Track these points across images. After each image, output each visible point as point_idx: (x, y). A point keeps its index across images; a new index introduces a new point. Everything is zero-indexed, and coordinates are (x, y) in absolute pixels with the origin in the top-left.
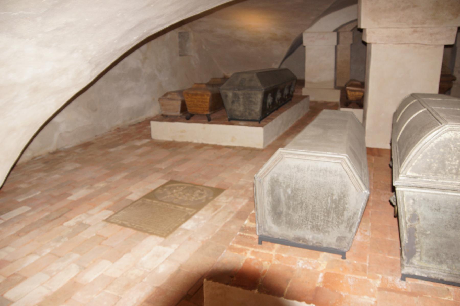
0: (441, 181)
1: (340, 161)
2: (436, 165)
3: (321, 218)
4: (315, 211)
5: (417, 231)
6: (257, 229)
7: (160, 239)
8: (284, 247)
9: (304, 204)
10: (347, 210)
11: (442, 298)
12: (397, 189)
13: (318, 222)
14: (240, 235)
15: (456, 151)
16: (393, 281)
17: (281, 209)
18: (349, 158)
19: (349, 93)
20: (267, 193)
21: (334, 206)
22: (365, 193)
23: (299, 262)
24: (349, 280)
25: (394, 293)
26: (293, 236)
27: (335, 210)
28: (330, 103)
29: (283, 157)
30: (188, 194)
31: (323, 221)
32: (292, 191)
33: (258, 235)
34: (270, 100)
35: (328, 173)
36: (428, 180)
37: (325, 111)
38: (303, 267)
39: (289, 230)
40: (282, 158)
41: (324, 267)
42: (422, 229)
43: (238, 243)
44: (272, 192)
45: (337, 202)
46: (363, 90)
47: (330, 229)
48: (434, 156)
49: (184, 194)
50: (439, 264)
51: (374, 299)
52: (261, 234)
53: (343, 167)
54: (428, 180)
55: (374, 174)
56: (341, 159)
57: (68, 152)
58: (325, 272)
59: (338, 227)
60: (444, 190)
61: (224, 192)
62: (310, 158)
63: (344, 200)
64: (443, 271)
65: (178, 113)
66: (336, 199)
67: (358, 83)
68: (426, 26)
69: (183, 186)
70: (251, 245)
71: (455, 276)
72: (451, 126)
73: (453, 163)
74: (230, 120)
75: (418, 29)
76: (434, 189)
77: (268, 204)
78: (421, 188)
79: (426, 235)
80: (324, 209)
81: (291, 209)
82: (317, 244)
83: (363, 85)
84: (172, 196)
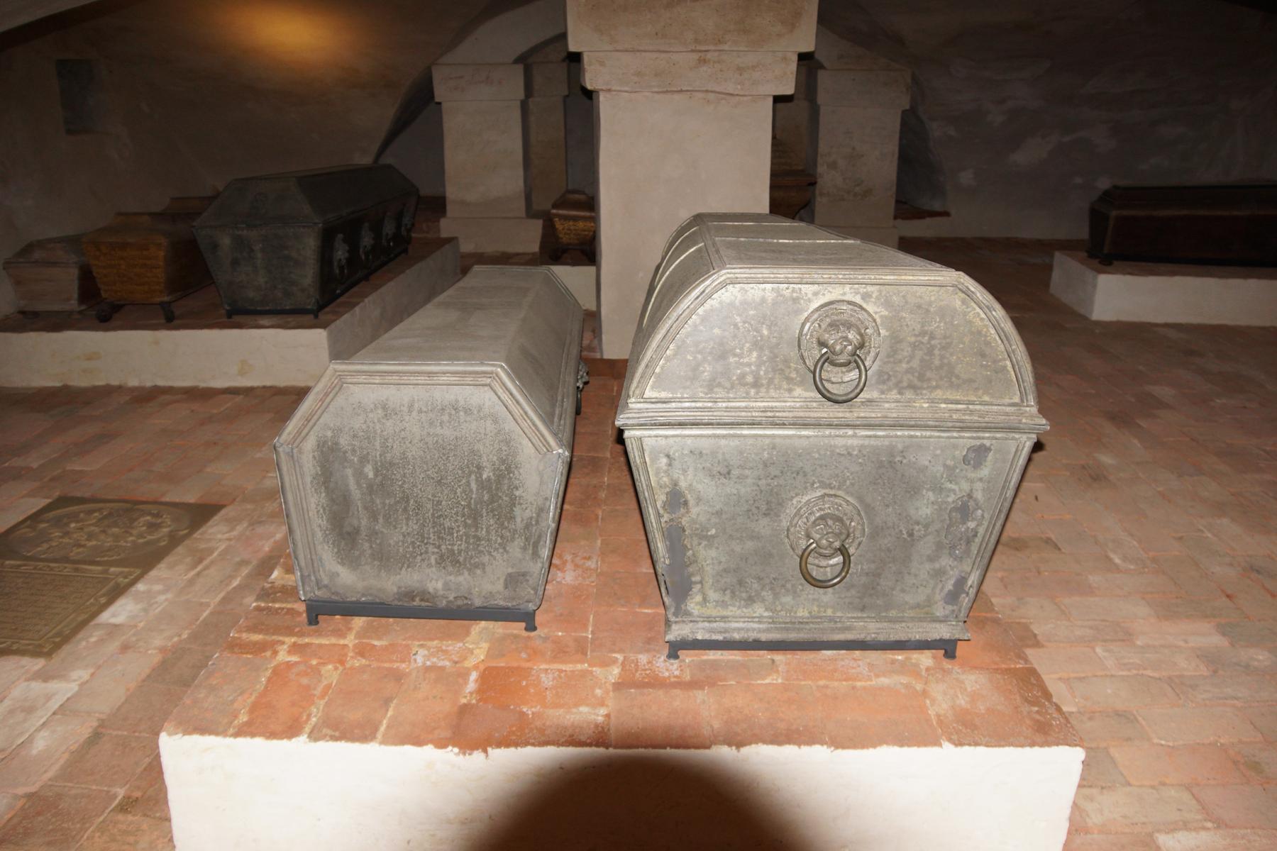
0: (724, 405)
1: (489, 381)
7: (38, 664)
8: (376, 621)
9: (412, 502)
11: (759, 682)
14: (258, 609)
16: (649, 662)
17: (355, 522)
19: (558, 224)
20: (312, 482)
26: (395, 590)
30: (115, 530)
34: (341, 253)
35: (462, 413)
36: (693, 405)
37: (476, 268)
38: (428, 663)
39: (383, 574)
43: (253, 629)
44: (326, 477)
47: (486, 559)
49: (104, 531)
52: (311, 595)
53: (496, 394)
54: (693, 405)
58: (482, 667)
59: (504, 548)
60: (732, 424)
61: (223, 512)
62: (413, 379)
65: (74, 305)
66: (489, 479)
68: (726, 47)
69: (100, 510)
70: (289, 631)
72: (730, 273)
74: (230, 315)
75: (709, 56)
77: (318, 512)
78: (681, 425)
81: (381, 520)
82: (460, 602)
83: (590, 204)
84: (66, 540)
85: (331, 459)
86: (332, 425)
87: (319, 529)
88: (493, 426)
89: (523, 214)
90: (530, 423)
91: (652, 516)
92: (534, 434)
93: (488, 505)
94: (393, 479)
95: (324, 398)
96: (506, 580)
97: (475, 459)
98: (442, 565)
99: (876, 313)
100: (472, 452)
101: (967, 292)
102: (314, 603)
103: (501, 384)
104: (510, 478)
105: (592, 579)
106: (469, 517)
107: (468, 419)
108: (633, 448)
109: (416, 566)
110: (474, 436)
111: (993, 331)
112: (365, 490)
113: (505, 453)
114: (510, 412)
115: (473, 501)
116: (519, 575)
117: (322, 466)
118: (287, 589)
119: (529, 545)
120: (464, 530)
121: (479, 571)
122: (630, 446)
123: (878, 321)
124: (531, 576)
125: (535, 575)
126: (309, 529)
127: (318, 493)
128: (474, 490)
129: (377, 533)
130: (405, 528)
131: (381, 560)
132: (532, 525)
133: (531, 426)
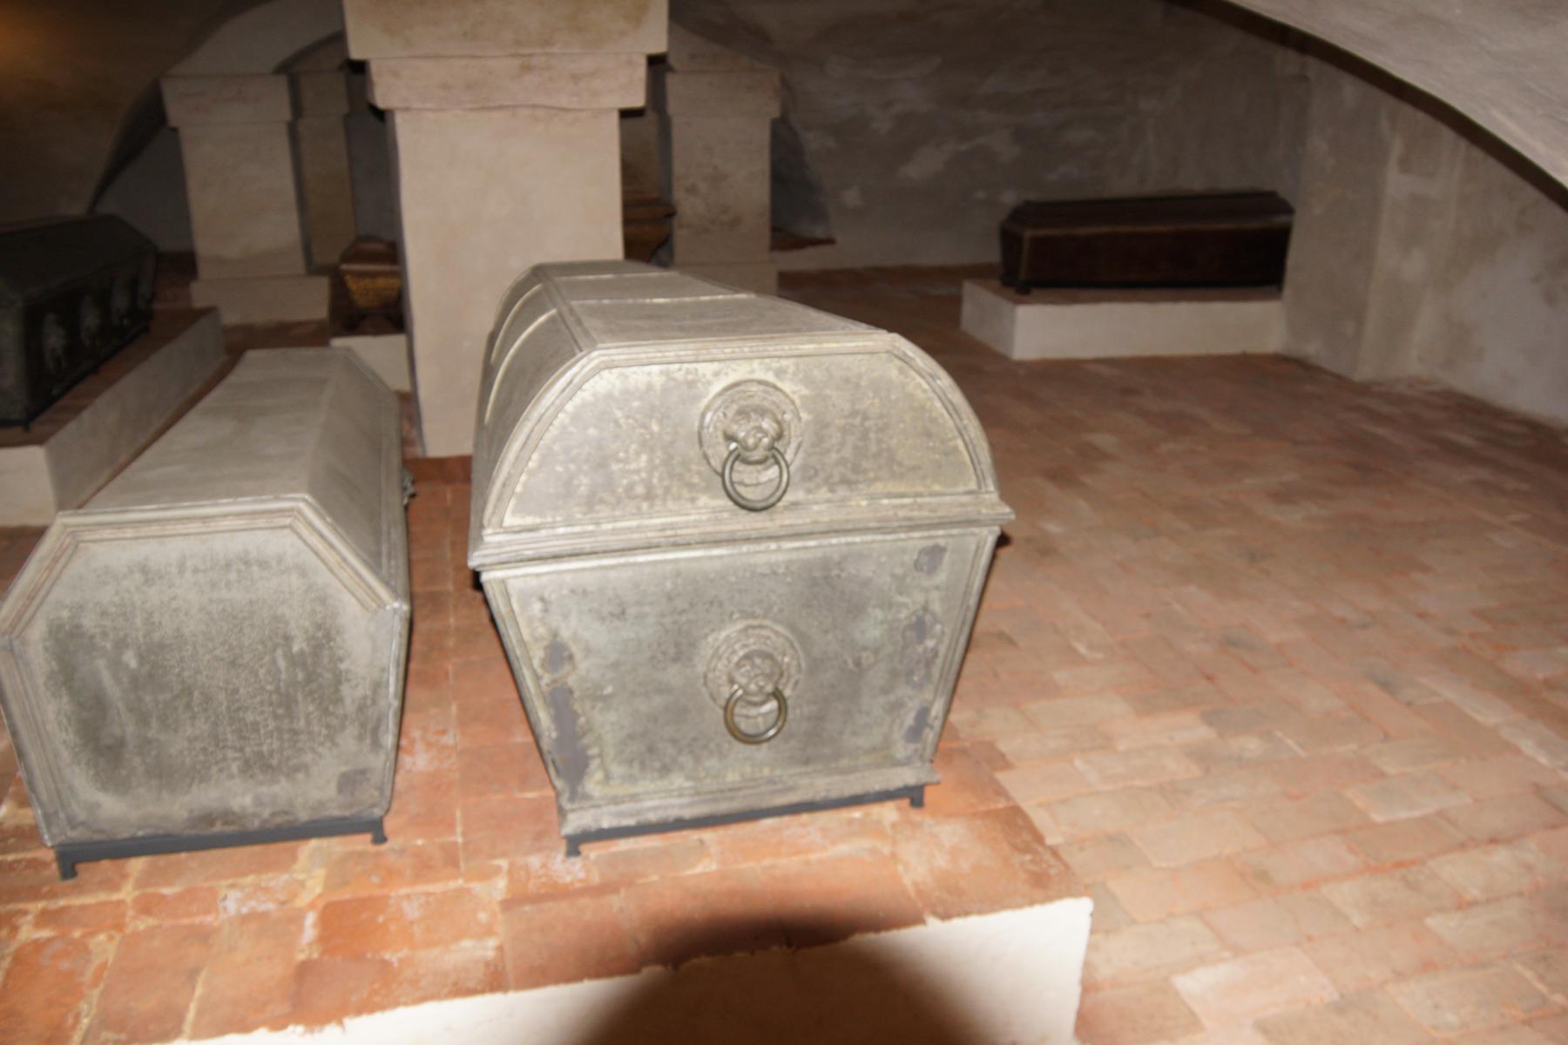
0: (610, 526)
1: (288, 521)
2: (585, 480)
3: (267, 726)
4: (239, 709)
5: (577, 694)
6: (43, 825)
8: (162, 860)
9: (196, 694)
10: (348, 680)
12: (484, 577)
13: (260, 745)
15: (634, 428)
16: (544, 866)
17: (117, 732)
18: (316, 505)
19: (352, 284)
20: (45, 684)
21: (300, 676)
22: (395, 611)
23: (225, 898)
24: (405, 905)
25: (550, 904)
26: (185, 814)
27: (307, 689)
28: (299, 324)
31: (275, 735)
32: (142, 659)
33: (52, 847)
34: (54, 339)
35: (255, 568)
37: (252, 355)
38: (244, 910)
40: (77, 547)
41: (318, 890)
42: (589, 685)
44: (67, 675)
45: (309, 661)
46: (396, 268)
47: (308, 758)
48: (574, 452)
50: (661, 777)
51: (492, 943)
53: (300, 537)
54: (569, 530)
56: (287, 514)
57: (528, 652)
58: (321, 904)
60: (623, 550)
62: (181, 528)
63: (331, 648)
64: (675, 793)
66: (302, 652)
67: (379, 247)
71: (710, 796)
73: (633, 466)
76: (593, 553)
77: (60, 724)
78: (557, 557)
79: (606, 699)
80: (271, 693)
82: (279, 820)
83: (393, 254)
99: (794, 392)
100: (276, 619)
101: (904, 359)
104: (331, 648)
111: (938, 404)
123: (798, 402)
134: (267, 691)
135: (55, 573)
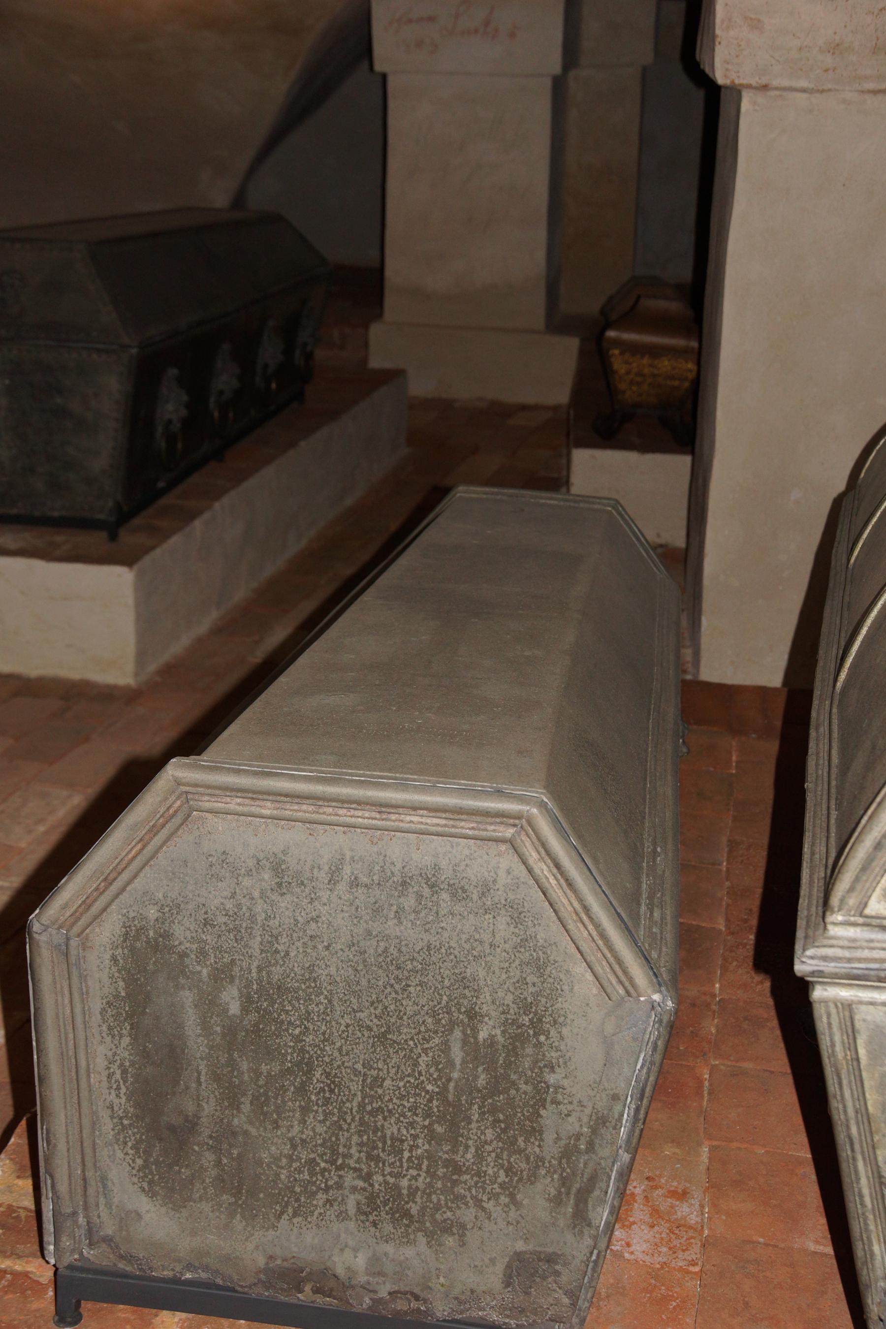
1: (509, 832)
17: (190, 1108)
19: (619, 364)
20: (103, 1011)
26: (261, 1261)
29: (192, 809)
35: (445, 896)
39: (238, 1223)
47: (468, 1214)
52: (69, 1258)
53: (524, 863)
55: (733, 845)
59: (512, 1196)
62: (344, 815)
66: (491, 1042)
77: (109, 1076)
81: (246, 1108)
82: (401, 1305)
85: (151, 967)
86: (161, 896)
87: (109, 1112)
88: (512, 929)
89: (540, 322)
90: (594, 933)
91: (864, 1181)
92: (599, 955)
93: (484, 1099)
94: (282, 1022)
95: (147, 837)
96: (508, 1266)
97: (465, 997)
98: (371, 1218)
100: (462, 980)
102: (77, 1274)
103: (537, 843)
104: (539, 1045)
105: (691, 1254)
106: (441, 1119)
107: (458, 908)
108: (830, 1024)
109: (312, 1212)
110: (467, 946)
112: (218, 1039)
113: (532, 989)
114: (551, 905)
115: (452, 1085)
116: (540, 1260)
117: (131, 981)
118: (18, 1218)
119: (568, 1194)
120: (427, 1147)
121: (451, 1239)
122: (825, 1020)
124: (565, 1264)
125: (577, 1261)
126: (85, 1110)
127: (113, 1036)
128: (458, 1061)
129: (234, 1134)
130: (296, 1128)
131: (237, 1193)
132: (579, 1152)
133: (596, 938)
134: (427, 1092)
135: (150, 848)
